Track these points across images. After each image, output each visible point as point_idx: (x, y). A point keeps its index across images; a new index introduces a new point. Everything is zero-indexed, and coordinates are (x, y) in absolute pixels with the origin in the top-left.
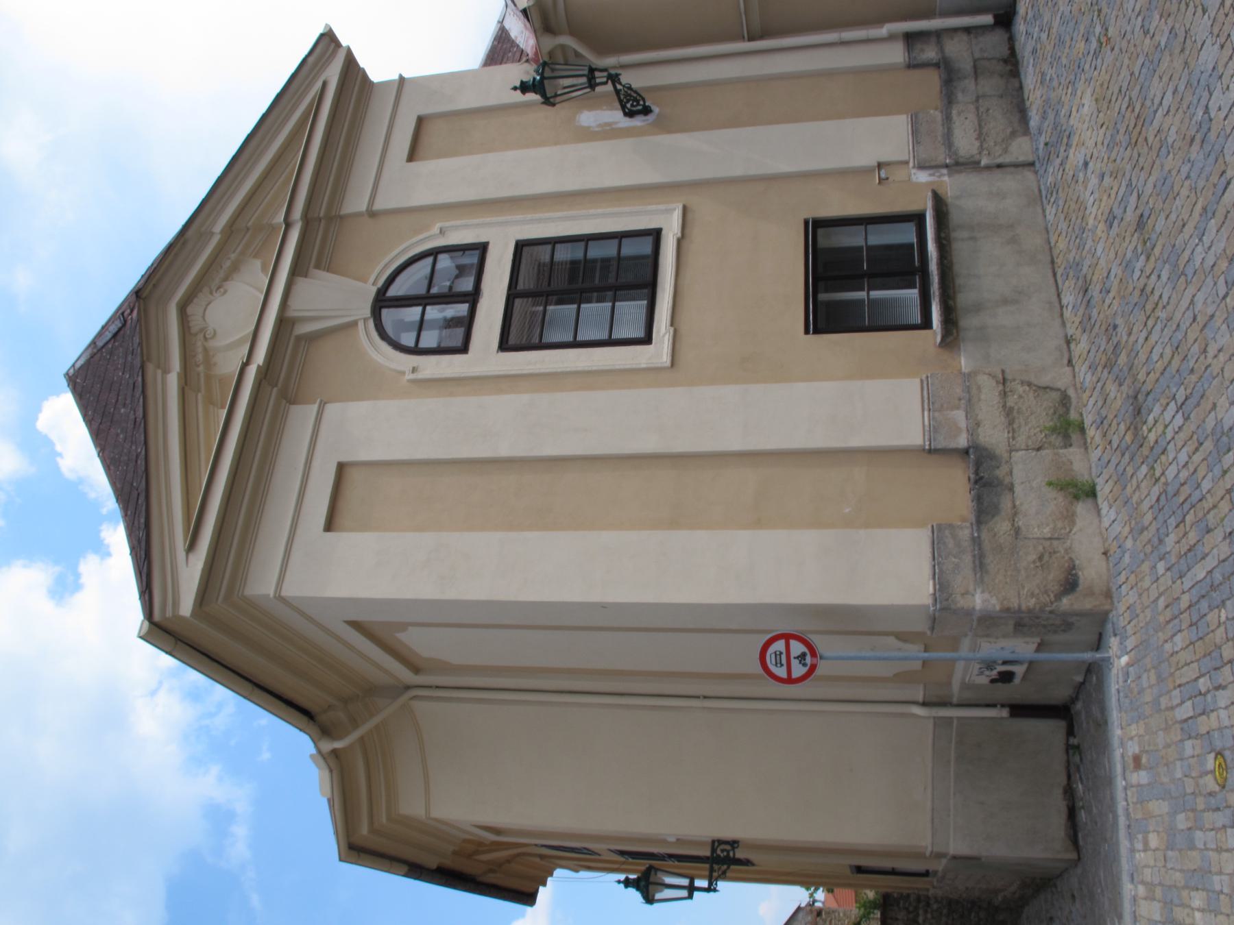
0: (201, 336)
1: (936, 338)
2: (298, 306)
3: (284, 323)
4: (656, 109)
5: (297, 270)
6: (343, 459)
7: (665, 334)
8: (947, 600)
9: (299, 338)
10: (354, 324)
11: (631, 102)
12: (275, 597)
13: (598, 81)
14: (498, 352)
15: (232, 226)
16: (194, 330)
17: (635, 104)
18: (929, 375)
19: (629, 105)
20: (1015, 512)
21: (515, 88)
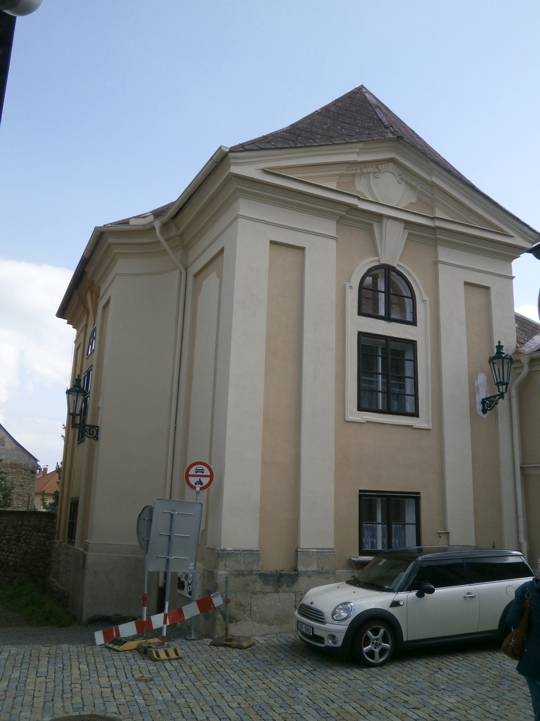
0: (376, 170)
1: (354, 557)
2: (389, 225)
3: (380, 217)
4: (485, 416)
5: (407, 223)
6: (307, 250)
7: (363, 418)
8: (223, 556)
9: (371, 225)
10: (377, 254)
11: (489, 403)
12: (238, 215)
13: (500, 387)
14: (358, 331)
15: (436, 186)
16: (380, 167)
17: (488, 405)
18: (335, 553)
19: (488, 402)
20: (265, 593)
21: (499, 342)
